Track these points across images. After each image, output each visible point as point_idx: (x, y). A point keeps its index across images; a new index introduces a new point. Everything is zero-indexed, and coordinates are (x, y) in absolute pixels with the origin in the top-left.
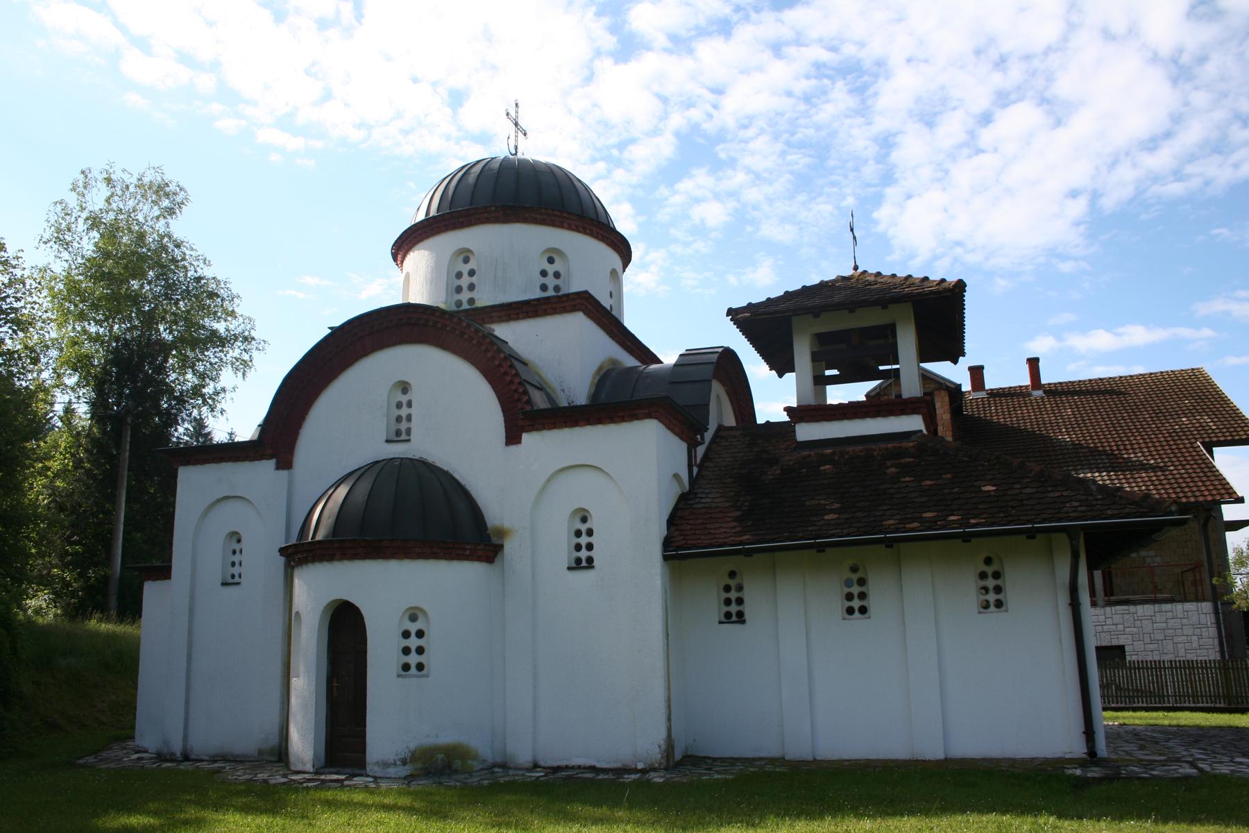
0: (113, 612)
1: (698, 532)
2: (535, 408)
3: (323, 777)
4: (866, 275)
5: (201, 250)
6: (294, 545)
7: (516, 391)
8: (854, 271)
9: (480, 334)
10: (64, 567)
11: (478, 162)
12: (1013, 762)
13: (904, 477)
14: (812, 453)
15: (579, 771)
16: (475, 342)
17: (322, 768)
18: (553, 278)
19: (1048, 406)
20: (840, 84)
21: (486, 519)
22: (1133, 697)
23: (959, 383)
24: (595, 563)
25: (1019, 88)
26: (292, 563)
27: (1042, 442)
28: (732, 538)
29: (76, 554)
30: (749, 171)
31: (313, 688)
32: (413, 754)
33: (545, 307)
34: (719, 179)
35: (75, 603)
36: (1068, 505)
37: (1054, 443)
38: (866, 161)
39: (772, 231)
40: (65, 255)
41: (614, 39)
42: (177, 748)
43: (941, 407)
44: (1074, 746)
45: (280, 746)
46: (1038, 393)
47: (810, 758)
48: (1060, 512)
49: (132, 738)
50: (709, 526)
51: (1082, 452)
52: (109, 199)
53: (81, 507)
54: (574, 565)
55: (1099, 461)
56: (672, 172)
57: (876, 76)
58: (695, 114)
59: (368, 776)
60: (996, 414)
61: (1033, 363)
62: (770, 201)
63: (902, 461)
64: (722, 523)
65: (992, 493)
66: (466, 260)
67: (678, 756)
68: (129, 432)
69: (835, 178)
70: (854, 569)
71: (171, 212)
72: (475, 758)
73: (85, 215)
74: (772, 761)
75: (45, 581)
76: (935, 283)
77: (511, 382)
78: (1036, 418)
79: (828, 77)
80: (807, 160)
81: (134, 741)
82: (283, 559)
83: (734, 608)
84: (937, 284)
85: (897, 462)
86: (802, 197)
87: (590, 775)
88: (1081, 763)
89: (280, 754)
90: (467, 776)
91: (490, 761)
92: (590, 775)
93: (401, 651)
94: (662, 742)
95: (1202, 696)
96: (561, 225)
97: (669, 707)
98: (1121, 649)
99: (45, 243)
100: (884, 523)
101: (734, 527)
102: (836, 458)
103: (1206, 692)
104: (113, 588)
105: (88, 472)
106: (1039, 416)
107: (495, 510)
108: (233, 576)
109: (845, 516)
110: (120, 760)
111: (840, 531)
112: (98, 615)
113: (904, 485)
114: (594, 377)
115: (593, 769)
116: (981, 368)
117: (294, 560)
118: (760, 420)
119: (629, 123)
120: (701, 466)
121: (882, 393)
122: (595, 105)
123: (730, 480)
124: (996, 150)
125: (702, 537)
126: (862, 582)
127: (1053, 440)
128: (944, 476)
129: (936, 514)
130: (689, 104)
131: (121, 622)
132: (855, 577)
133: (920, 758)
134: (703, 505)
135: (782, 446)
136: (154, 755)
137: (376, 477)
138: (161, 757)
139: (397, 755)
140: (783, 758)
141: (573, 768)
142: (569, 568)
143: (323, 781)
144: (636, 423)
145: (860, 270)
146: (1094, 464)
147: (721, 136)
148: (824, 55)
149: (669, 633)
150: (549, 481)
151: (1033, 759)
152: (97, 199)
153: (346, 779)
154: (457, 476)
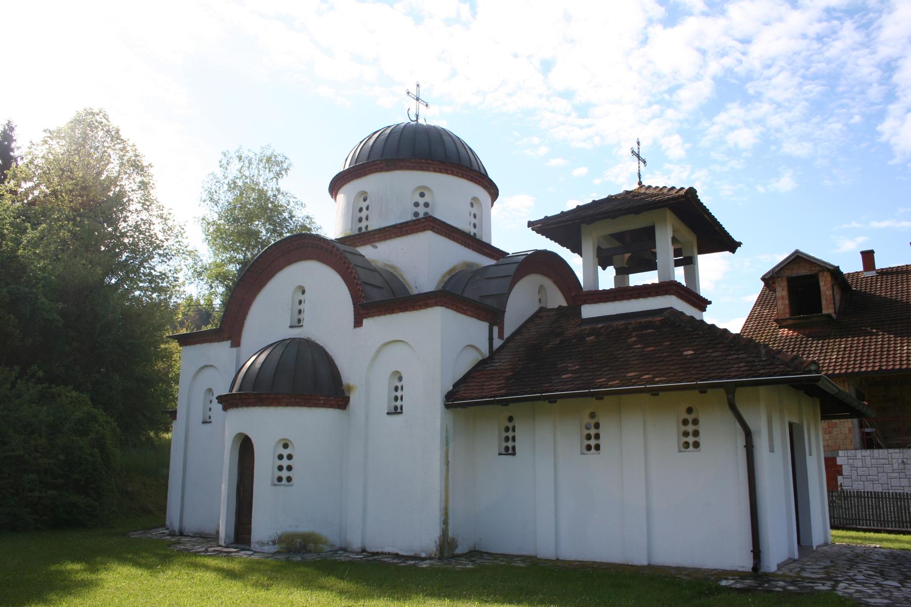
5: (301, 198)
11: (389, 127)
13: (637, 345)
17: (231, 544)
18: (423, 207)
21: (342, 379)
23: (837, 266)
30: (772, 101)
33: (406, 229)
36: (735, 366)
38: (871, 84)
39: (792, 148)
41: (663, 9)
43: (825, 285)
44: (745, 562)
48: (725, 372)
52: (241, 169)
54: (393, 411)
57: (880, 12)
58: (728, 61)
60: (881, 290)
62: (790, 124)
63: (644, 332)
66: (422, 195)
69: (844, 101)
71: (278, 175)
72: (325, 543)
79: (838, 19)
80: (820, 88)
86: (815, 120)
90: (821, 585)
91: (338, 545)
94: (437, 539)
96: (427, 169)
109: (576, 375)
114: (444, 276)
115: (397, 556)
118: (708, 306)
119: (676, 73)
121: (775, 276)
122: (650, 62)
126: (597, 426)
128: (664, 344)
130: (723, 54)
132: (593, 422)
133: (629, 564)
139: (270, 538)
140: (536, 557)
142: (388, 413)
147: (749, 77)
149: (450, 459)
150: (378, 351)
154: (328, 350)
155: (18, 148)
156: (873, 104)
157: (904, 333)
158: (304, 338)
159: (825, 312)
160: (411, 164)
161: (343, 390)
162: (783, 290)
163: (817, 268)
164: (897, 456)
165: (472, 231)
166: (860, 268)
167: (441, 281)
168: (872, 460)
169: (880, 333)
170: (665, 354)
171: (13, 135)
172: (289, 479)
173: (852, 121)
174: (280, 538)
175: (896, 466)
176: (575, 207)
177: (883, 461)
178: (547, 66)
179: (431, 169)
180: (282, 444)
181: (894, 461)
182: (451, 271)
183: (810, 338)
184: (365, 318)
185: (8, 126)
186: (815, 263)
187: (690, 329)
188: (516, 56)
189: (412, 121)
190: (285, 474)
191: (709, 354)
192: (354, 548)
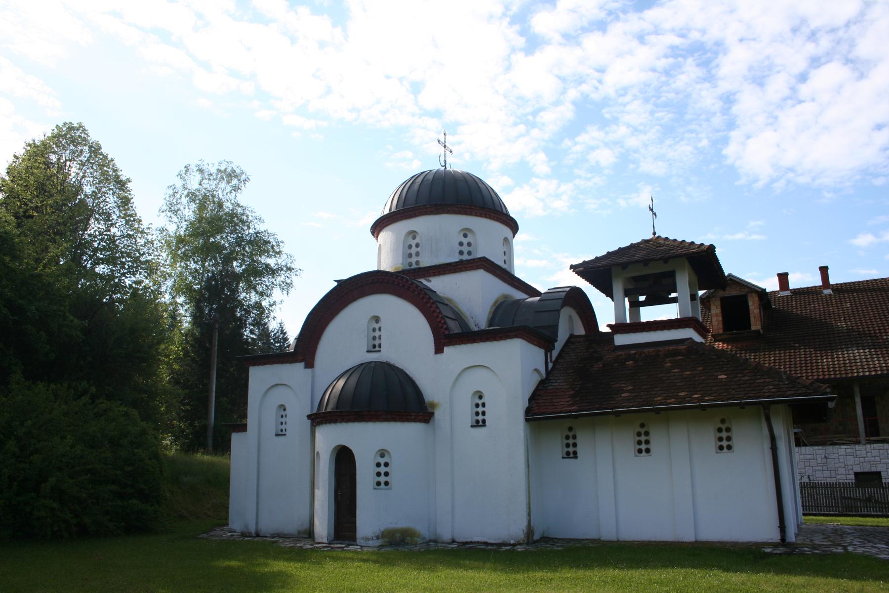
0: (210, 449)
1: (547, 404)
2: (451, 333)
3: (333, 546)
4: (659, 239)
6: (315, 414)
7: (440, 322)
8: (653, 236)
9: (419, 289)
10: (180, 419)
12: (735, 544)
13: (674, 369)
14: (623, 353)
15: (477, 544)
16: (416, 293)
19: (834, 301)
20: (690, 60)
21: (424, 397)
22: (882, 507)
25: (828, 54)
26: (314, 424)
27: (825, 327)
28: (566, 408)
29: (186, 411)
30: (628, 126)
31: (327, 495)
32: (383, 533)
34: (607, 133)
35: (188, 442)
36: (766, 388)
37: (834, 328)
38: (714, 114)
39: (649, 166)
40: (175, 219)
42: (253, 530)
45: (310, 528)
46: (828, 292)
47: (616, 540)
48: (760, 393)
49: (227, 525)
50: (554, 400)
51: (853, 335)
53: (189, 381)
54: (475, 424)
55: (865, 341)
56: (572, 130)
57: (716, 54)
59: (357, 545)
61: (824, 270)
62: (646, 146)
63: (675, 358)
64: (562, 399)
65: (724, 380)
66: (465, 236)
67: (536, 537)
68: (217, 334)
70: (642, 425)
71: (236, 189)
72: (419, 536)
73: (186, 192)
74: (593, 541)
75: (169, 429)
76: (696, 246)
77: (437, 316)
78: (823, 310)
80: (670, 116)
81: (228, 527)
82: (310, 421)
83: (571, 449)
84: (698, 247)
85: (673, 359)
86: (668, 142)
87: (484, 547)
88: (775, 545)
89: (310, 533)
90: (414, 546)
91: (428, 538)
92: (484, 547)
93: (375, 475)
94: (525, 528)
95: (832, 507)
96: (470, 214)
97: (529, 508)
98: (878, 474)
99: (163, 212)
100: (655, 399)
101: (569, 401)
102: (637, 357)
103: (829, 504)
104: (210, 433)
105: (193, 360)
106: (826, 309)
107: (431, 389)
108: (282, 430)
109: (634, 394)
110: (221, 536)
111: (628, 404)
112: (202, 450)
113: (673, 374)
114: (492, 308)
115: (486, 543)
116: (787, 274)
117: (315, 422)
120: (555, 363)
122: (514, 86)
123: (572, 371)
124: (813, 100)
125: (549, 407)
127: (833, 326)
128: (698, 369)
129: (686, 393)
131: (216, 454)
134: (553, 387)
135: (607, 348)
136: (239, 534)
137: (361, 374)
138: (243, 534)
139: (374, 534)
140: (600, 539)
141: (475, 543)
143: (333, 548)
144: (509, 341)
145: (656, 236)
146: (861, 343)
147: (605, 102)
148: (677, 41)
150: (460, 375)
151: (748, 542)
152: (193, 183)
153: (345, 547)
154: (407, 372)
156: (718, 131)
157: (817, 348)
158: (384, 361)
159: (753, 328)
160: (456, 209)
161: (426, 406)
162: (717, 308)
163: (746, 290)
164: (821, 452)
165: (504, 266)
166: (777, 288)
167: (490, 313)
168: (801, 456)
169: (802, 347)
170: (703, 377)
173: (700, 145)
174: (382, 533)
175: (819, 460)
176: (606, 253)
177: (809, 456)
178: (416, 88)
179: (473, 213)
181: (818, 456)
182: (496, 302)
183: (743, 350)
184: (447, 346)
186: (745, 285)
187: (715, 357)
188: (388, 77)
190: (382, 479)
191: (740, 378)
192: (445, 539)
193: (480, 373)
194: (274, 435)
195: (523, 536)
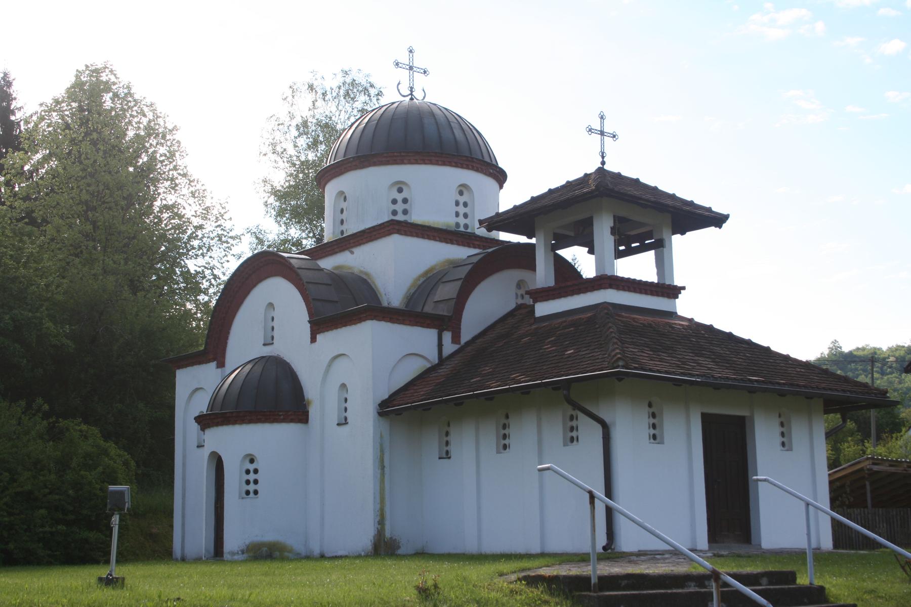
24: (349, 420)
32: (248, 547)
66: (400, 190)
94: (372, 538)
114: (418, 279)
118: (682, 291)
142: (338, 424)
149: (386, 463)
150: (330, 365)
155: (20, 109)
167: (413, 285)
171: (11, 91)
172: (256, 492)
180: (250, 457)
182: (426, 273)
185: (4, 81)
189: (404, 96)
190: (252, 487)
193: (340, 364)
194: (196, 447)
195: (371, 547)
